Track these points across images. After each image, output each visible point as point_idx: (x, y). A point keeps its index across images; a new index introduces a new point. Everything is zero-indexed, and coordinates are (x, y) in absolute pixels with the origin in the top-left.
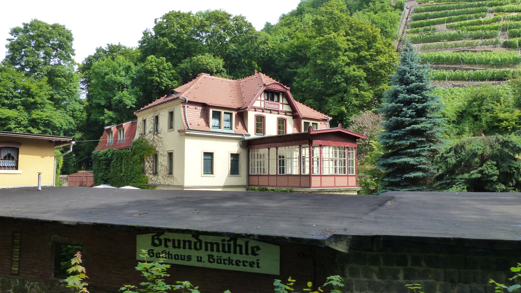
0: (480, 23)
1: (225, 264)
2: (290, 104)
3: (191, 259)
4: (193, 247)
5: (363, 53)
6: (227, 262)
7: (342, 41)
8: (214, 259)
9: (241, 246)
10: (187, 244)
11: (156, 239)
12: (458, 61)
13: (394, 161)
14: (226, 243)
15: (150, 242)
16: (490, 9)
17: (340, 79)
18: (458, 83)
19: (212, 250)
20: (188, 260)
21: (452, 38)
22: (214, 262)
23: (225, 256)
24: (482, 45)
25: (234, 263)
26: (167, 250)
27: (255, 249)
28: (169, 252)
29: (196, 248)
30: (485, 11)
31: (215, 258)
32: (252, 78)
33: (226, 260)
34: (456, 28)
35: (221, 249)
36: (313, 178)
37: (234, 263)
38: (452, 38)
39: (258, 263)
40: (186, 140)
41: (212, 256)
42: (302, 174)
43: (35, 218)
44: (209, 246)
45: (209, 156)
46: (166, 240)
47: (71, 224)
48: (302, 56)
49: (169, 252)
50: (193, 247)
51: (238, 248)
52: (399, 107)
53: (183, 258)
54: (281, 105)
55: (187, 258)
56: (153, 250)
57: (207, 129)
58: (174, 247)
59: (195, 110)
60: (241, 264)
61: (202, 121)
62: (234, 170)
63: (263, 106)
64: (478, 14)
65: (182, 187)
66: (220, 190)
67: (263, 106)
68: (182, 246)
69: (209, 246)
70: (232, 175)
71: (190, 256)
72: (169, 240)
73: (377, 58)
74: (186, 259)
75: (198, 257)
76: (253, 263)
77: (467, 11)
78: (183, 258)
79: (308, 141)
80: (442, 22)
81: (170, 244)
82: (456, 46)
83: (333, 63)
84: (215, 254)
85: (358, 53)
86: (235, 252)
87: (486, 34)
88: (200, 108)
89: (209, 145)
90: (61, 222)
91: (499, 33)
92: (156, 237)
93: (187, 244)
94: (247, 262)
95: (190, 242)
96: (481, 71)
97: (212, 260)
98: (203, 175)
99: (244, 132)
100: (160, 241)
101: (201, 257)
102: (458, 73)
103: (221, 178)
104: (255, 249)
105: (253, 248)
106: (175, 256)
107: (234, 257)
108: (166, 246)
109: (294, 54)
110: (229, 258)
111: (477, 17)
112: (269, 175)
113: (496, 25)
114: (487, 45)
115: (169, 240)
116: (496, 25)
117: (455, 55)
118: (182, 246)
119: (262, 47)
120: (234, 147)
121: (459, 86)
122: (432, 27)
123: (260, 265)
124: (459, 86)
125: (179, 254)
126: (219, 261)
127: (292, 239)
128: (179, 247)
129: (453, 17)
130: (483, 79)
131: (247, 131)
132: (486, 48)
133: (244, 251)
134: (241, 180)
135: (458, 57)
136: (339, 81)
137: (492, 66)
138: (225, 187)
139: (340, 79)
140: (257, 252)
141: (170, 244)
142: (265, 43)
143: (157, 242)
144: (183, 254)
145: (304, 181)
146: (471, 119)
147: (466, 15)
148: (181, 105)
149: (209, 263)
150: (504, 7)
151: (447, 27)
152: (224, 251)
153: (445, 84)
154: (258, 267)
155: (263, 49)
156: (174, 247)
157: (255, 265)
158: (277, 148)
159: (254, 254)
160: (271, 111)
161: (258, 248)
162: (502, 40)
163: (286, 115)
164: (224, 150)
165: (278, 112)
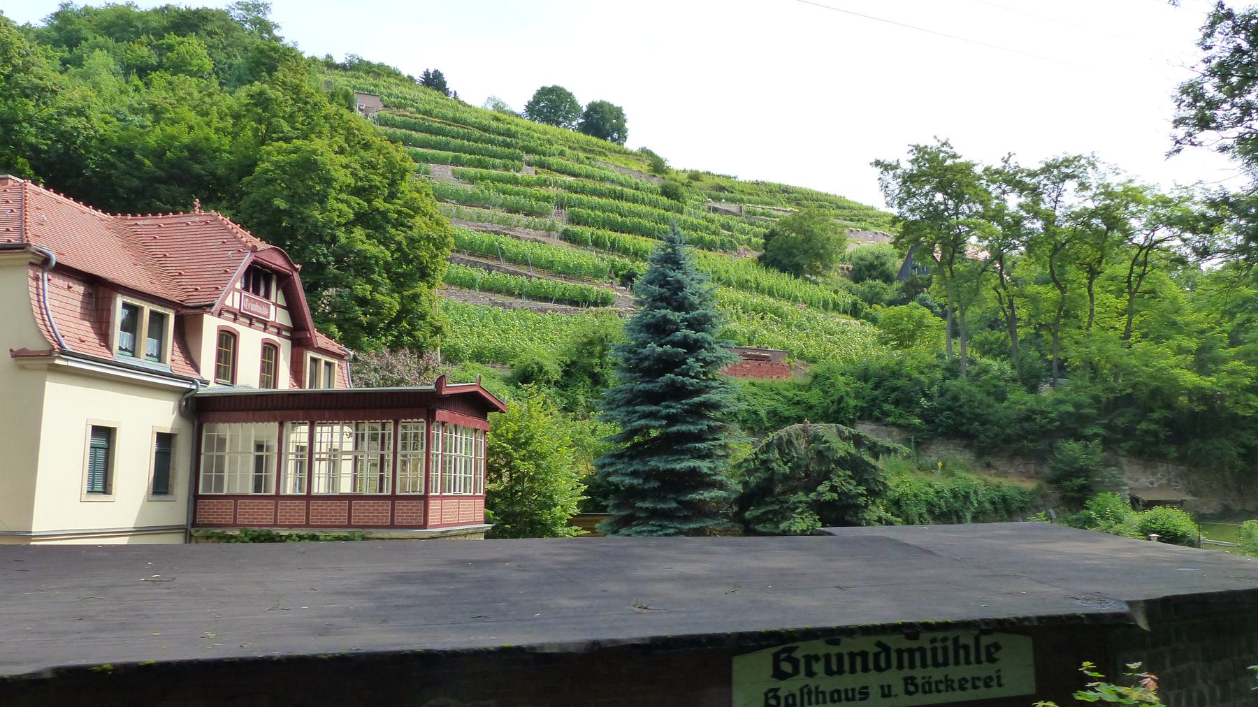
0: (516, 182)
1: (938, 691)
2: (292, 306)
3: (867, 694)
4: (871, 665)
5: (379, 203)
6: (942, 687)
7: (340, 169)
8: (916, 686)
9: (966, 647)
10: (859, 660)
11: (784, 660)
12: (493, 253)
13: (669, 466)
14: (939, 645)
15: (769, 670)
16: (526, 157)
17: (325, 256)
18: (499, 298)
19: (912, 666)
20: (861, 699)
21: (469, 201)
22: (917, 691)
23: (937, 674)
24: (527, 227)
25: (956, 686)
26: (812, 683)
27: (993, 650)
28: (817, 688)
29: (878, 668)
30: (519, 159)
31: (919, 681)
32: (188, 220)
33: (941, 682)
34: (472, 180)
35: (929, 660)
36: (434, 505)
37: (956, 686)
38: (469, 201)
39: (999, 678)
40: (47, 383)
41: (913, 678)
42: (398, 493)
43: (260, 654)
44: (906, 656)
45: (104, 435)
46: (810, 659)
47: (571, 650)
48: (199, 176)
49: (817, 688)
50: (871, 665)
51: (962, 653)
52: (677, 354)
53: (850, 695)
54: (273, 308)
55: (860, 693)
56: (776, 690)
57: (103, 354)
58: (829, 672)
59: (67, 293)
60: (969, 685)
61: (86, 329)
62: (161, 485)
63: (237, 306)
64: (509, 162)
65: (28, 536)
66: (123, 541)
67: (237, 306)
68: (847, 667)
69: (906, 656)
70: (157, 497)
71: (866, 688)
72: (817, 658)
73: (410, 222)
74: (857, 696)
75: (882, 687)
76: (990, 678)
77: (487, 150)
78: (850, 695)
79: (425, 410)
80: (443, 162)
81: (818, 667)
82: (479, 219)
83: (316, 213)
84: (919, 673)
85: (369, 201)
86: (853, 671)
87: (532, 206)
88: (79, 289)
89: (108, 405)
90: (532, 648)
91: (554, 210)
92: (783, 656)
93: (859, 660)
94: (979, 679)
95: (864, 655)
96: (549, 283)
97: (912, 688)
98: (84, 497)
99: (190, 372)
100: (795, 663)
101: (889, 687)
102: (498, 277)
103: (128, 506)
104: (993, 650)
105: (988, 647)
106: (832, 693)
107: (956, 672)
108: (810, 673)
109: (177, 164)
110: (946, 677)
111: (506, 168)
112: (277, 497)
113: (543, 191)
114: (535, 229)
115: (817, 658)
116: (543, 191)
117: (487, 238)
118: (847, 667)
119: (71, 122)
120: (162, 414)
121: (503, 305)
122: (424, 166)
123: (1003, 681)
124: (503, 305)
125: (842, 688)
126: (927, 688)
127: (1040, 619)
128: (840, 671)
129: (463, 155)
130: (546, 299)
131: (198, 370)
132: (533, 234)
133: (972, 657)
134: (174, 511)
135: (492, 245)
136: (322, 259)
137: (558, 274)
138: (139, 531)
139: (325, 256)
140: (996, 656)
141: (818, 667)
142: (80, 113)
143: (786, 667)
144: (849, 687)
145: (404, 512)
146: (588, 381)
147: (487, 159)
148: (31, 273)
149: (908, 698)
150: (551, 160)
151: (454, 173)
152: (936, 664)
153: (474, 297)
154: (1000, 685)
155: (75, 128)
156: (829, 672)
157: (994, 683)
158: (281, 424)
159: (991, 659)
160: (251, 320)
161: (997, 647)
162: (562, 225)
163: (279, 334)
164: (144, 419)
165: (265, 325)
